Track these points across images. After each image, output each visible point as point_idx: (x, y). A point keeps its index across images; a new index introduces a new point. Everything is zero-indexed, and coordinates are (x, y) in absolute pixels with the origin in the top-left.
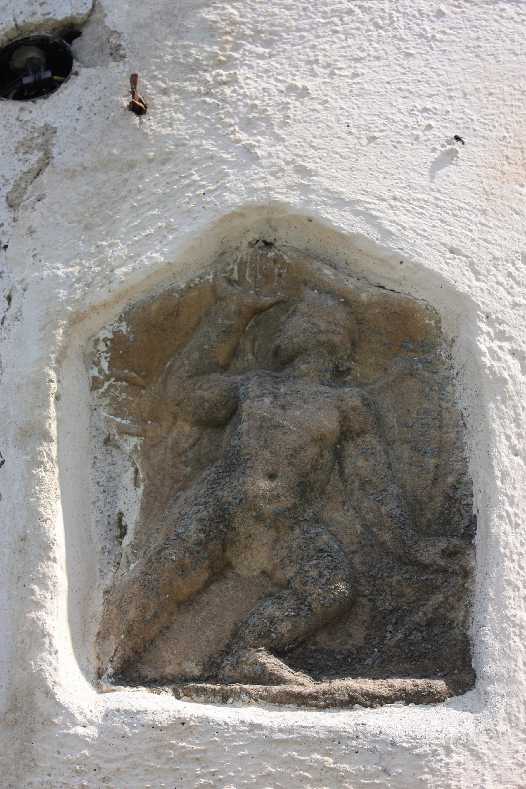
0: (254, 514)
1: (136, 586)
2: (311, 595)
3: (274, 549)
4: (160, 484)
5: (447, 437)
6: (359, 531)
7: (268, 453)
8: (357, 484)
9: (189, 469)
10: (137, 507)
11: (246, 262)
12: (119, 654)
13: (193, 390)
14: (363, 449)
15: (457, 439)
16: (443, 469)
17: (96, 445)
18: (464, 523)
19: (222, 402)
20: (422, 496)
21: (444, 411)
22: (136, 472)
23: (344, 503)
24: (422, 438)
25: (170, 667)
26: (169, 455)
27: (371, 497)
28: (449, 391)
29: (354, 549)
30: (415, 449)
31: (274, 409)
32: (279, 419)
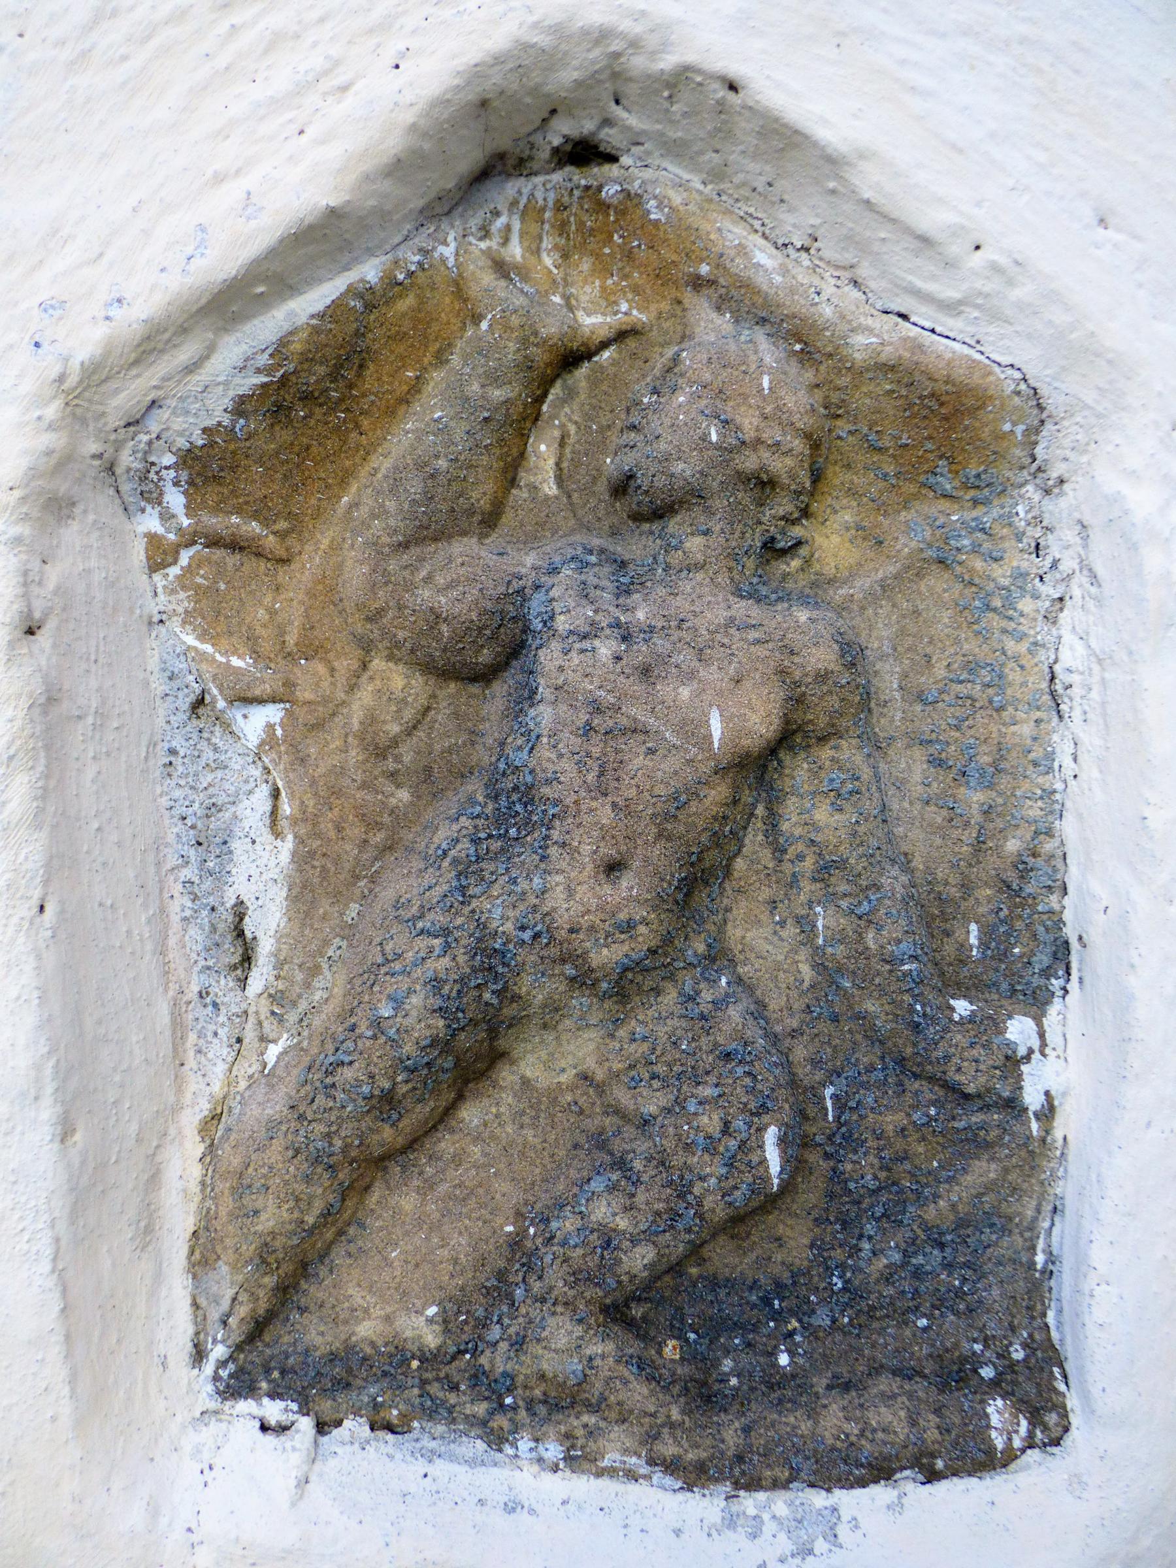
0: (570, 971)
1: (278, 1144)
2: (702, 1179)
3: (612, 1036)
4: (332, 834)
5: (1014, 734)
6: (807, 979)
7: (608, 808)
8: (809, 863)
9: (404, 795)
10: (279, 894)
11: (543, 209)
12: (243, 1311)
13: (410, 587)
14: (832, 780)
15: (1035, 739)
16: (999, 815)
17: (172, 718)
18: (1041, 962)
19: (486, 627)
20: (947, 883)
21: (1011, 664)
22: (276, 794)
23: (773, 904)
24: (958, 734)
25: (367, 1324)
26: (355, 755)
27: (844, 904)
28: (1026, 610)
29: (795, 1024)
30: (937, 762)
31: (622, 678)
32: (637, 712)
